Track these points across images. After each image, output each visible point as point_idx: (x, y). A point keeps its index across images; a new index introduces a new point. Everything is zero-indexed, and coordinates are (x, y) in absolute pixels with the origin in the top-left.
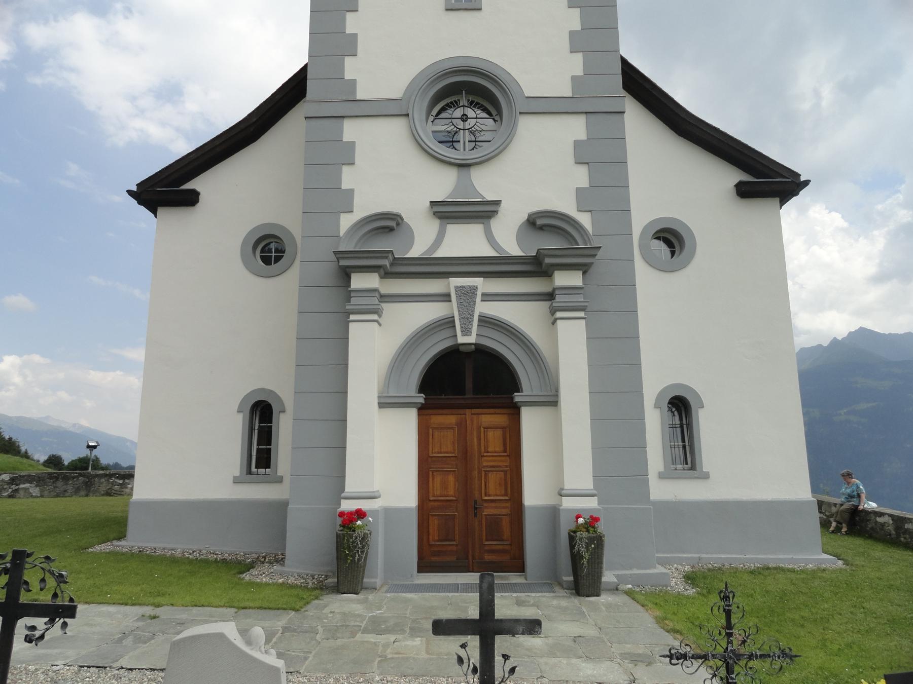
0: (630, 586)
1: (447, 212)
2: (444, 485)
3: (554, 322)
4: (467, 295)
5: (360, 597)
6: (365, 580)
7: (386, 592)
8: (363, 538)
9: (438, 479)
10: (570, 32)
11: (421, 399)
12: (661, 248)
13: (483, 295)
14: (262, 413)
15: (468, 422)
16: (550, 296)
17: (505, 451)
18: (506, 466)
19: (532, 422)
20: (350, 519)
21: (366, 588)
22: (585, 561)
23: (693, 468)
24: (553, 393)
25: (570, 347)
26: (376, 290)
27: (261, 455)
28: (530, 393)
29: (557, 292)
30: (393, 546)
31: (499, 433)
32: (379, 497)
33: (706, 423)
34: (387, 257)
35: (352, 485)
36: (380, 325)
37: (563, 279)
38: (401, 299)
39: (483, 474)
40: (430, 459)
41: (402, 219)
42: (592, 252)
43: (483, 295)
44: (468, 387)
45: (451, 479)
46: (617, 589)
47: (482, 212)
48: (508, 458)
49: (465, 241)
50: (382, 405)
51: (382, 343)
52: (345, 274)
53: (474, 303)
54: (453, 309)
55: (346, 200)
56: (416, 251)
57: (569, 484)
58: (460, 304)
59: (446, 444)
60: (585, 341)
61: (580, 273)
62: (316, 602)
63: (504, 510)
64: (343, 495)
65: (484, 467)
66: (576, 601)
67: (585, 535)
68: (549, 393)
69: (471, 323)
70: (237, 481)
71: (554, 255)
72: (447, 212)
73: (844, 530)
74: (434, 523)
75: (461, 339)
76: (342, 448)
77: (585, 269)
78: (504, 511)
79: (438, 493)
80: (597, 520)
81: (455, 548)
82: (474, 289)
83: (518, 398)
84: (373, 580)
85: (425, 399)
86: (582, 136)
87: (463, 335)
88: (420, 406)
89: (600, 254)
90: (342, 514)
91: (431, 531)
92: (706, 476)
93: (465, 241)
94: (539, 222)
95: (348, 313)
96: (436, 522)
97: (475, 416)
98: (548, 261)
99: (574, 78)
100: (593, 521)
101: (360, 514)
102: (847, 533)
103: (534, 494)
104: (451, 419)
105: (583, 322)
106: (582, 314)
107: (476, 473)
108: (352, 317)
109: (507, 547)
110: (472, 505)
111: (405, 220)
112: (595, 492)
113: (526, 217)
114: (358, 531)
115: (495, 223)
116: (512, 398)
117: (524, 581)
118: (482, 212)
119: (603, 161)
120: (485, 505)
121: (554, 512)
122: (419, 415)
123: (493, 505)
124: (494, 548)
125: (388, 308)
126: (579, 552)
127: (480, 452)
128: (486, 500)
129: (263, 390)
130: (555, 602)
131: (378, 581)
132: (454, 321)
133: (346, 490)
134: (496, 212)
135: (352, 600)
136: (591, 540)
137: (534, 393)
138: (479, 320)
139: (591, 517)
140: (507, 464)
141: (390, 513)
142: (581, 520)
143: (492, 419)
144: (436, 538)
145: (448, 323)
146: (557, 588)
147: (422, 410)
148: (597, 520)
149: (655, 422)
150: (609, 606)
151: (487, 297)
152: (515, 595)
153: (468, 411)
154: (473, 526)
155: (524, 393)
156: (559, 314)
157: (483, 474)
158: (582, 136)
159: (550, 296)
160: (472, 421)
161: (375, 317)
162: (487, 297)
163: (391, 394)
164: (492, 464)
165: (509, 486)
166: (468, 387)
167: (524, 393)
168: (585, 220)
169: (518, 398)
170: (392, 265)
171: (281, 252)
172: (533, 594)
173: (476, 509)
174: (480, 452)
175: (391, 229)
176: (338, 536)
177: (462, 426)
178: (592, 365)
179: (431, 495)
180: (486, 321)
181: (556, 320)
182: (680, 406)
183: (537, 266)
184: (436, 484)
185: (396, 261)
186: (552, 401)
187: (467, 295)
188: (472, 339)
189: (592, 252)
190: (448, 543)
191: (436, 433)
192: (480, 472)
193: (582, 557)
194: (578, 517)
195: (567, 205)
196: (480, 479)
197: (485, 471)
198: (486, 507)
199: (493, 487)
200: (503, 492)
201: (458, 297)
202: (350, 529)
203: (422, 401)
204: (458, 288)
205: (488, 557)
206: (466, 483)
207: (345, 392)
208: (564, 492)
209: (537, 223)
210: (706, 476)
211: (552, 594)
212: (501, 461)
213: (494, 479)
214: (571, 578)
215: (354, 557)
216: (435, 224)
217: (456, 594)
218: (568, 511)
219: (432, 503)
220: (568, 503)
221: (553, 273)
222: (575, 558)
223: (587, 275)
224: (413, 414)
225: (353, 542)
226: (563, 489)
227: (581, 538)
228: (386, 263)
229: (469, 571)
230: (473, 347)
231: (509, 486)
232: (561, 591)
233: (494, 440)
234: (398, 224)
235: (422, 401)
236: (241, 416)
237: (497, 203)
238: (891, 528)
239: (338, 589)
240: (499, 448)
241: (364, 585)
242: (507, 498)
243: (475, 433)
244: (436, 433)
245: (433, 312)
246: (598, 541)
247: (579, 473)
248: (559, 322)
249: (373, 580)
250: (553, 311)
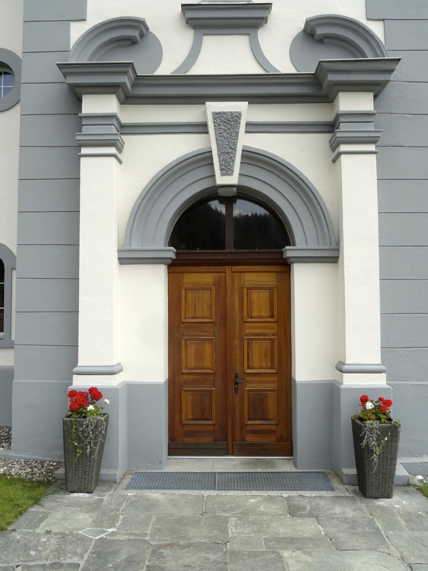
0: (420, 477)
2: (199, 356)
3: (335, 160)
4: (228, 124)
5: (94, 497)
6: (103, 471)
7: (129, 487)
8: (96, 427)
9: (192, 349)
10: (169, 454)
11: (171, 253)
13: (248, 124)
15: (229, 282)
16: (331, 127)
17: (272, 316)
18: (274, 334)
19: (305, 281)
20: (81, 401)
21: (104, 482)
22: (375, 458)
24: (334, 246)
26: (113, 116)
28: (304, 247)
29: (342, 119)
30: (137, 431)
31: (264, 295)
32: (121, 371)
34: (126, 73)
35: (88, 355)
36: (120, 162)
37: (350, 103)
38: (146, 130)
39: (246, 342)
40: (182, 326)
41: (147, 29)
42: (388, 66)
43: (248, 124)
44: (229, 243)
45: (208, 348)
46: (409, 485)
48: (275, 325)
49: (225, 56)
50: (122, 261)
51: (119, 186)
52: (76, 94)
53: (237, 134)
54: (211, 141)
55: (266, 215)
56: (166, 68)
57: (352, 358)
58: (218, 135)
59: (202, 307)
60: (375, 182)
61: (371, 95)
62: (35, 509)
63: (270, 385)
64: (76, 369)
65: (247, 335)
66: (363, 505)
67: (376, 424)
68: (328, 247)
69: (232, 159)
74: (188, 400)
75: (221, 180)
76: (73, 312)
77: (376, 89)
78: (270, 386)
79: (193, 365)
80: (388, 403)
81: (212, 429)
82: (236, 117)
83: (289, 252)
84: (112, 472)
85: (177, 254)
87: (223, 175)
88: (170, 262)
89: (398, 67)
90: (72, 394)
91: (184, 409)
93: (225, 56)
94: (320, 31)
95: (81, 145)
96: (190, 398)
97: (236, 274)
98: (331, 77)
100: (383, 405)
101: (95, 394)
103: (307, 367)
104: (206, 278)
105: (373, 157)
106: (372, 148)
107: (237, 342)
108: (84, 151)
109: (274, 428)
110: (230, 377)
111: (151, 30)
112: (383, 367)
113: (302, 26)
114: (90, 418)
116: (282, 253)
117: (294, 470)
120: (248, 379)
121: (330, 392)
122: (169, 273)
123: (257, 378)
124: (258, 428)
125: (130, 141)
126: (367, 446)
127: (242, 317)
128: (249, 374)
130: (338, 510)
131: (119, 473)
132: (211, 158)
133: (79, 364)
134: (263, 20)
135: (78, 504)
136: (384, 431)
137: (309, 247)
138: (243, 156)
139: (381, 399)
140: (274, 331)
141: (132, 389)
142: (369, 405)
143: (256, 278)
144: (190, 417)
145: (204, 159)
146: (335, 483)
147: (173, 267)
148: (388, 403)
150: (409, 518)
151: (254, 127)
152: (285, 494)
153: (228, 269)
154: (233, 402)
155: (298, 246)
156: (343, 148)
157: (246, 342)
159: (331, 127)
160: (233, 280)
161: (113, 150)
163: (134, 247)
164: (257, 331)
165: (276, 357)
166: (229, 243)
167: (298, 246)
168: (377, 29)
169: (289, 252)
170: (133, 85)
172: (307, 494)
173: (237, 383)
174: (242, 317)
175: (132, 42)
176: (65, 423)
177: (221, 289)
179: (183, 367)
180: (252, 157)
181: (340, 154)
183: (316, 89)
184: (190, 353)
185: (140, 81)
186: (331, 256)
188: (233, 179)
189: (388, 66)
190: (204, 422)
191: (190, 295)
192: (242, 340)
193: (371, 452)
194: (364, 400)
195: (356, 12)
196: (242, 349)
197: (248, 339)
198: (249, 382)
199: (258, 358)
200: (269, 364)
201: (217, 126)
202: (81, 413)
203: (172, 255)
204: (217, 115)
205: (250, 439)
206: (225, 353)
207: (76, 245)
208: (345, 367)
209: (318, 32)
211: (330, 494)
212: (268, 328)
213: (258, 350)
214: (353, 471)
215: (84, 449)
216: (189, 35)
217: (213, 493)
218: (350, 390)
219: (185, 377)
220: (350, 381)
221: (336, 95)
222: (361, 455)
223: (378, 98)
224: (161, 271)
225: (84, 432)
226: (344, 364)
227: (371, 429)
228: (125, 80)
229: (227, 454)
230: (235, 189)
231: (276, 357)
232: (341, 486)
233: (260, 302)
234: (142, 35)
235: (172, 255)
237: (267, 7)
239: (66, 486)
240: (265, 312)
241: (101, 478)
242: (274, 371)
243: (236, 295)
244: (190, 295)
245: (185, 145)
246: (392, 431)
247: (364, 345)
248: (343, 157)
249: (112, 472)
250: (334, 145)
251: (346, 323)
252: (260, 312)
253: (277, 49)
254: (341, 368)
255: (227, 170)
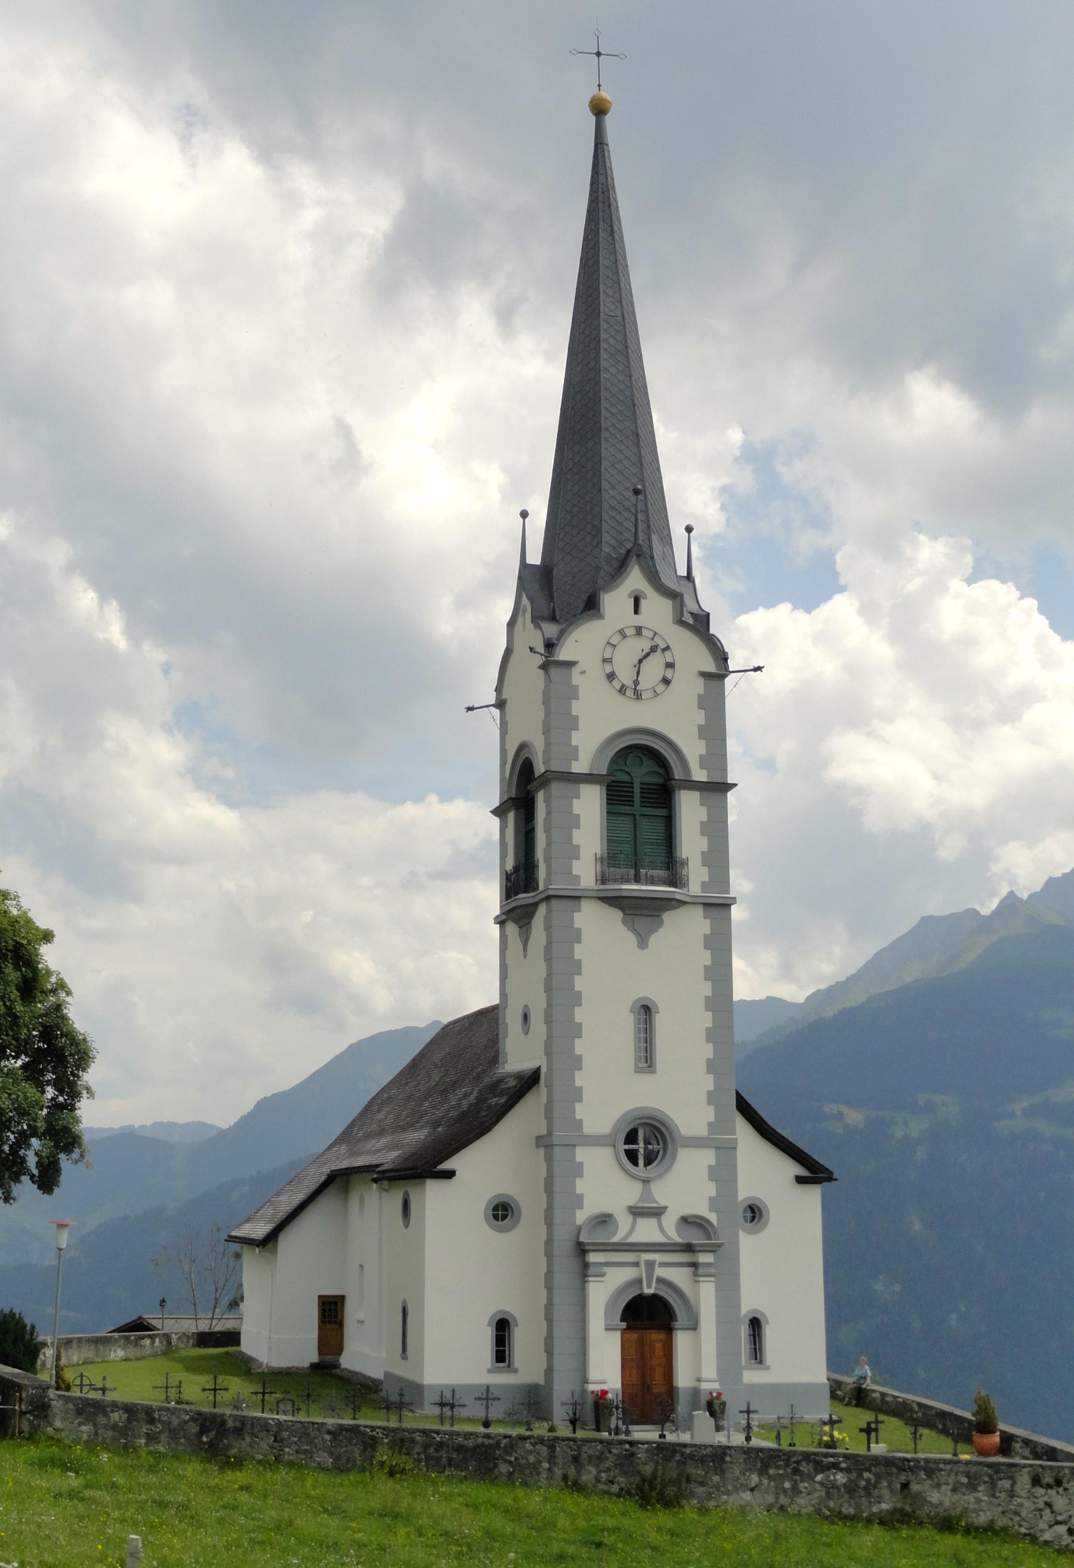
1: (637, 1212)
4: (650, 1265)
12: (749, 1214)
14: (502, 1328)
16: (694, 1265)
19: (682, 1340)
23: (761, 1362)
25: (706, 1297)
27: (502, 1354)
33: (769, 1334)
35: (592, 1375)
37: (704, 1258)
44: (649, 1317)
47: (657, 1213)
49: (647, 1231)
50: (607, 1329)
51: (603, 1294)
55: (578, 1201)
57: (704, 1376)
70: (489, 1371)
71: (698, 1242)
72: (637, 1212)
73: (854, 1402)
86: (712, 1162)
92: (768, 1368)
99: (709, 1124)
100: (719, 1395)
102: (856, 1406)
103: (683, 1379)
106: (713, 1279)
110: (646, 1387)
115: (664, 1218)
118: (657, 1213)
119: (724, 1174)
121: (695, 1392)
129: (500, 1312)
143: (656, 1336)
145: (639, 1281)
149: (744, 1331)
151: (662, 1265)
158: (712, 1162)
162: (662, 1265)
166: (649, 1317)
171: (496, 1208)
175: (605, 1222)
178: (717, 1306)
180: (661, 1281)
182: (755, 1324)
186: (694, 1327)
187: (650, 1265)
199: (658, 1377)
210: (768, 1368)
216: (631, 1217)
220: (705, 1386)
224: (618, 1334)
233: (659, 1346)
236: (490, 1328)
237: (666, 1208)
238: (879, 1401)
240: (661, 1353)
246: (724, 1404)
250: (696, 1274)
251: (703, 1352)
252: (263, 1401)
253: (671, 1230)
254: (699, 1380)
255: (649, 1286)
